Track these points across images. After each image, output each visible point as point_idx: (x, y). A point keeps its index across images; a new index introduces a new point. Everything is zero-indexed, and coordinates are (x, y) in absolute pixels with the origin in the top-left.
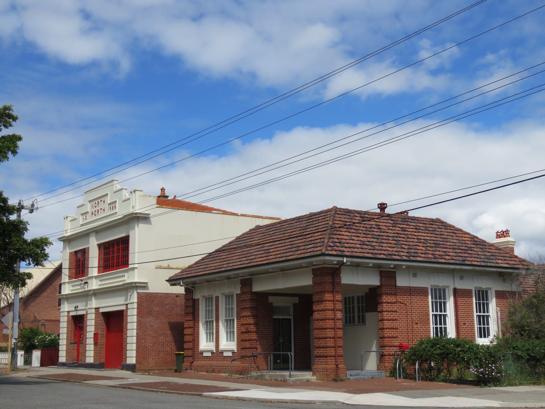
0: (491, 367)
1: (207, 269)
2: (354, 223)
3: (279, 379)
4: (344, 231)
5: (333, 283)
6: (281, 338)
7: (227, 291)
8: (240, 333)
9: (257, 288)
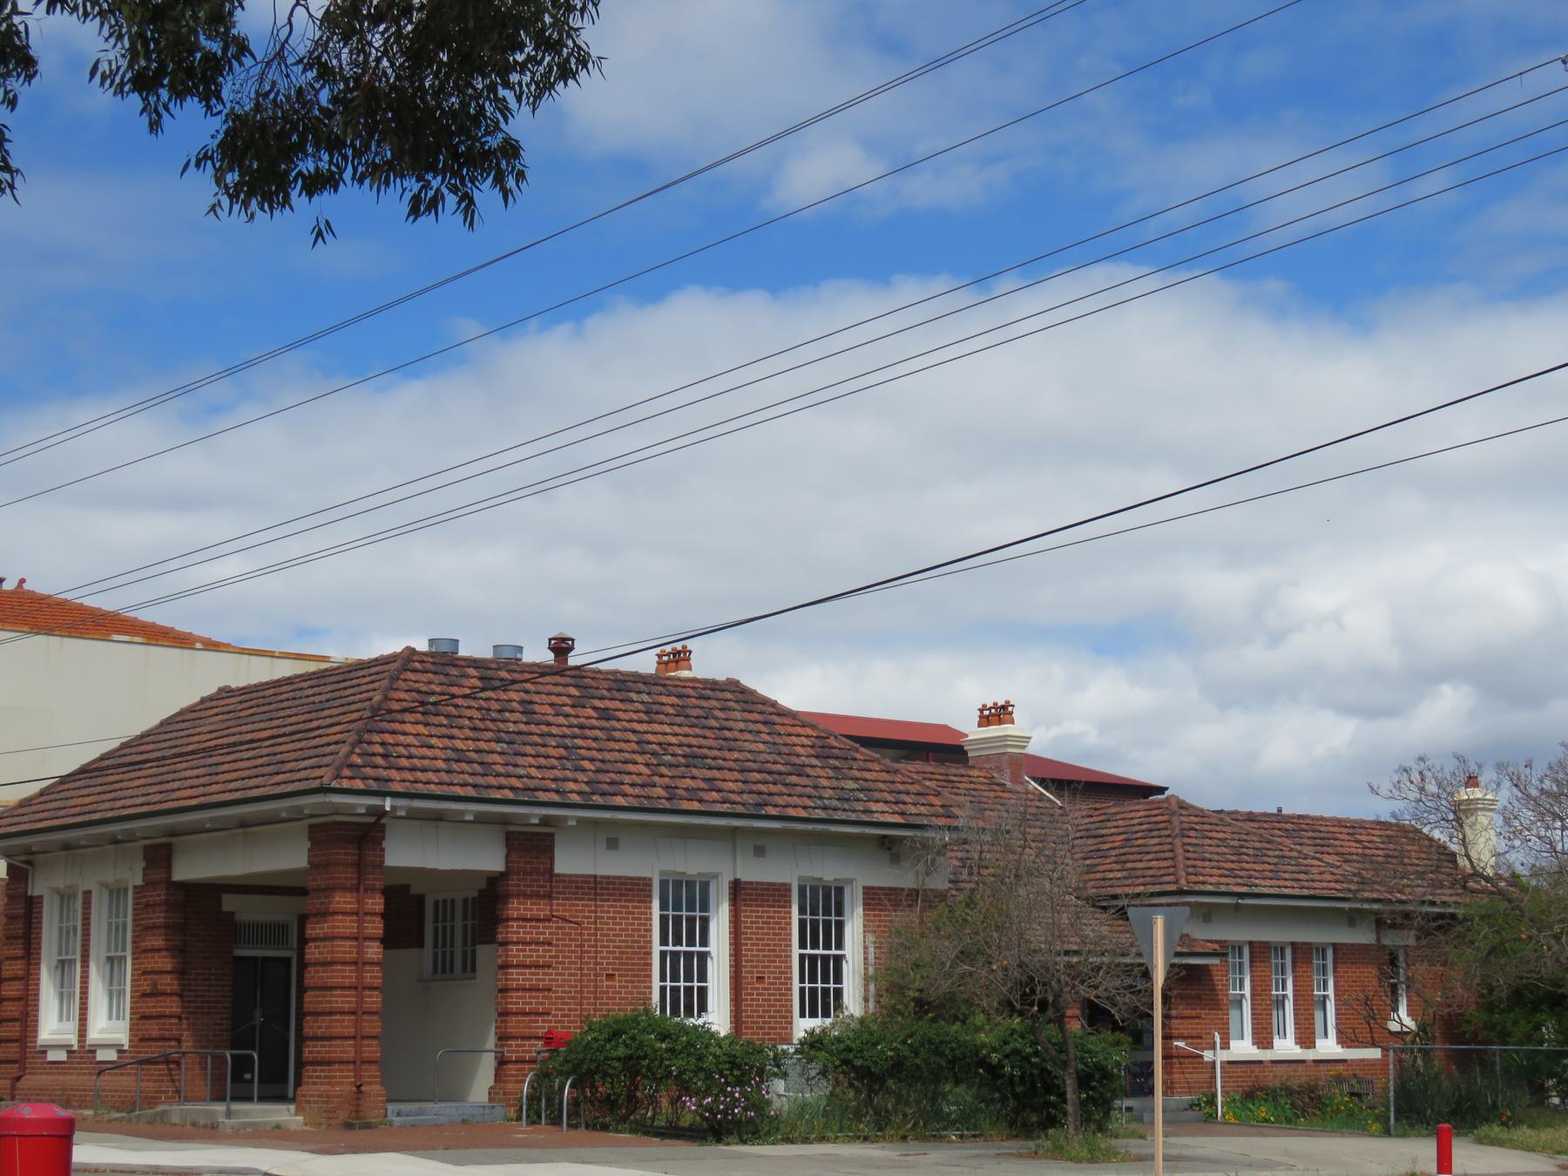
0: (732, 1094)
1: (61, 813)
2: (453, 696)
3: (202, 1122)
4: (412, 727)
5: (359, 866)
6: (258, 1012)
7: (110, 876)
8: (140, 996)
9: (187, 870)
